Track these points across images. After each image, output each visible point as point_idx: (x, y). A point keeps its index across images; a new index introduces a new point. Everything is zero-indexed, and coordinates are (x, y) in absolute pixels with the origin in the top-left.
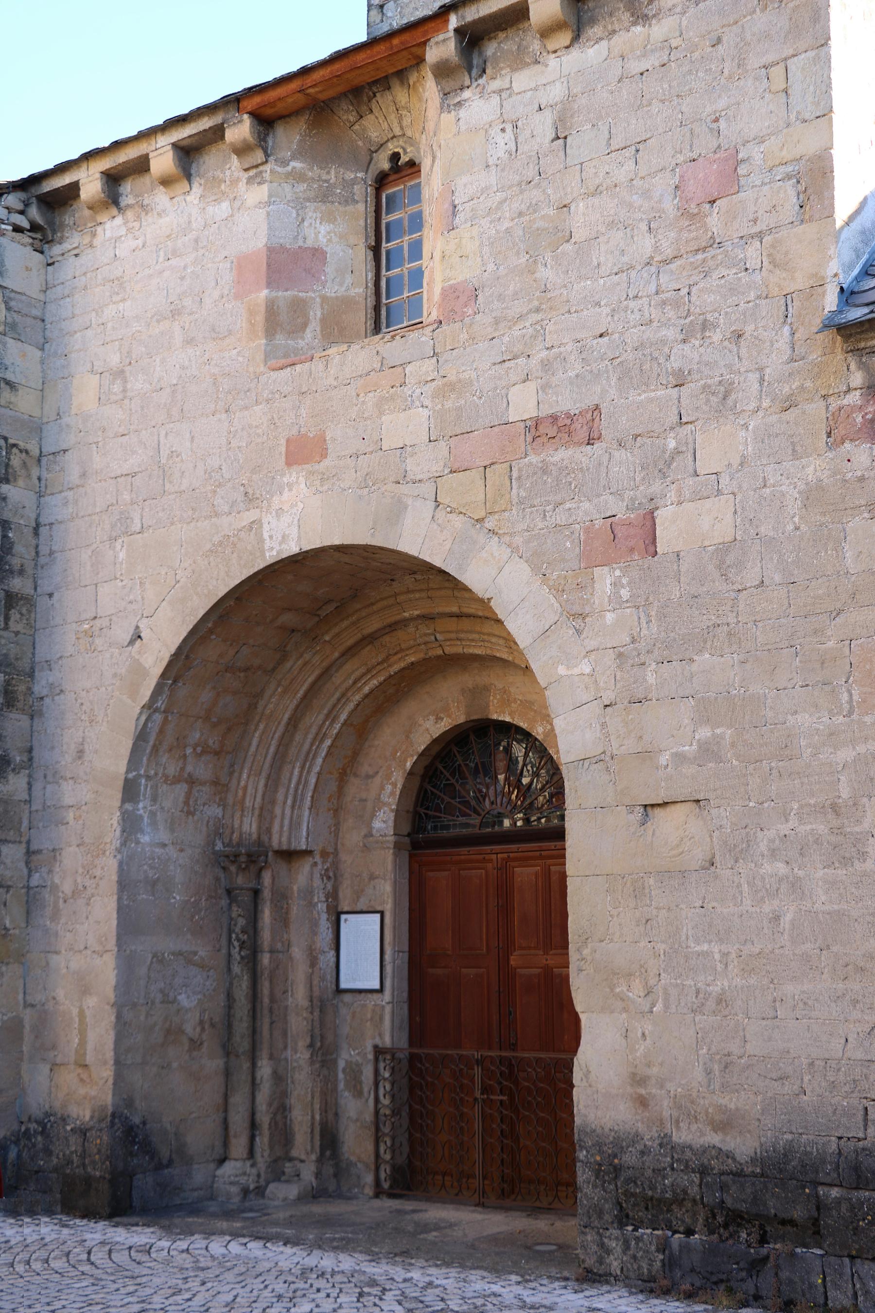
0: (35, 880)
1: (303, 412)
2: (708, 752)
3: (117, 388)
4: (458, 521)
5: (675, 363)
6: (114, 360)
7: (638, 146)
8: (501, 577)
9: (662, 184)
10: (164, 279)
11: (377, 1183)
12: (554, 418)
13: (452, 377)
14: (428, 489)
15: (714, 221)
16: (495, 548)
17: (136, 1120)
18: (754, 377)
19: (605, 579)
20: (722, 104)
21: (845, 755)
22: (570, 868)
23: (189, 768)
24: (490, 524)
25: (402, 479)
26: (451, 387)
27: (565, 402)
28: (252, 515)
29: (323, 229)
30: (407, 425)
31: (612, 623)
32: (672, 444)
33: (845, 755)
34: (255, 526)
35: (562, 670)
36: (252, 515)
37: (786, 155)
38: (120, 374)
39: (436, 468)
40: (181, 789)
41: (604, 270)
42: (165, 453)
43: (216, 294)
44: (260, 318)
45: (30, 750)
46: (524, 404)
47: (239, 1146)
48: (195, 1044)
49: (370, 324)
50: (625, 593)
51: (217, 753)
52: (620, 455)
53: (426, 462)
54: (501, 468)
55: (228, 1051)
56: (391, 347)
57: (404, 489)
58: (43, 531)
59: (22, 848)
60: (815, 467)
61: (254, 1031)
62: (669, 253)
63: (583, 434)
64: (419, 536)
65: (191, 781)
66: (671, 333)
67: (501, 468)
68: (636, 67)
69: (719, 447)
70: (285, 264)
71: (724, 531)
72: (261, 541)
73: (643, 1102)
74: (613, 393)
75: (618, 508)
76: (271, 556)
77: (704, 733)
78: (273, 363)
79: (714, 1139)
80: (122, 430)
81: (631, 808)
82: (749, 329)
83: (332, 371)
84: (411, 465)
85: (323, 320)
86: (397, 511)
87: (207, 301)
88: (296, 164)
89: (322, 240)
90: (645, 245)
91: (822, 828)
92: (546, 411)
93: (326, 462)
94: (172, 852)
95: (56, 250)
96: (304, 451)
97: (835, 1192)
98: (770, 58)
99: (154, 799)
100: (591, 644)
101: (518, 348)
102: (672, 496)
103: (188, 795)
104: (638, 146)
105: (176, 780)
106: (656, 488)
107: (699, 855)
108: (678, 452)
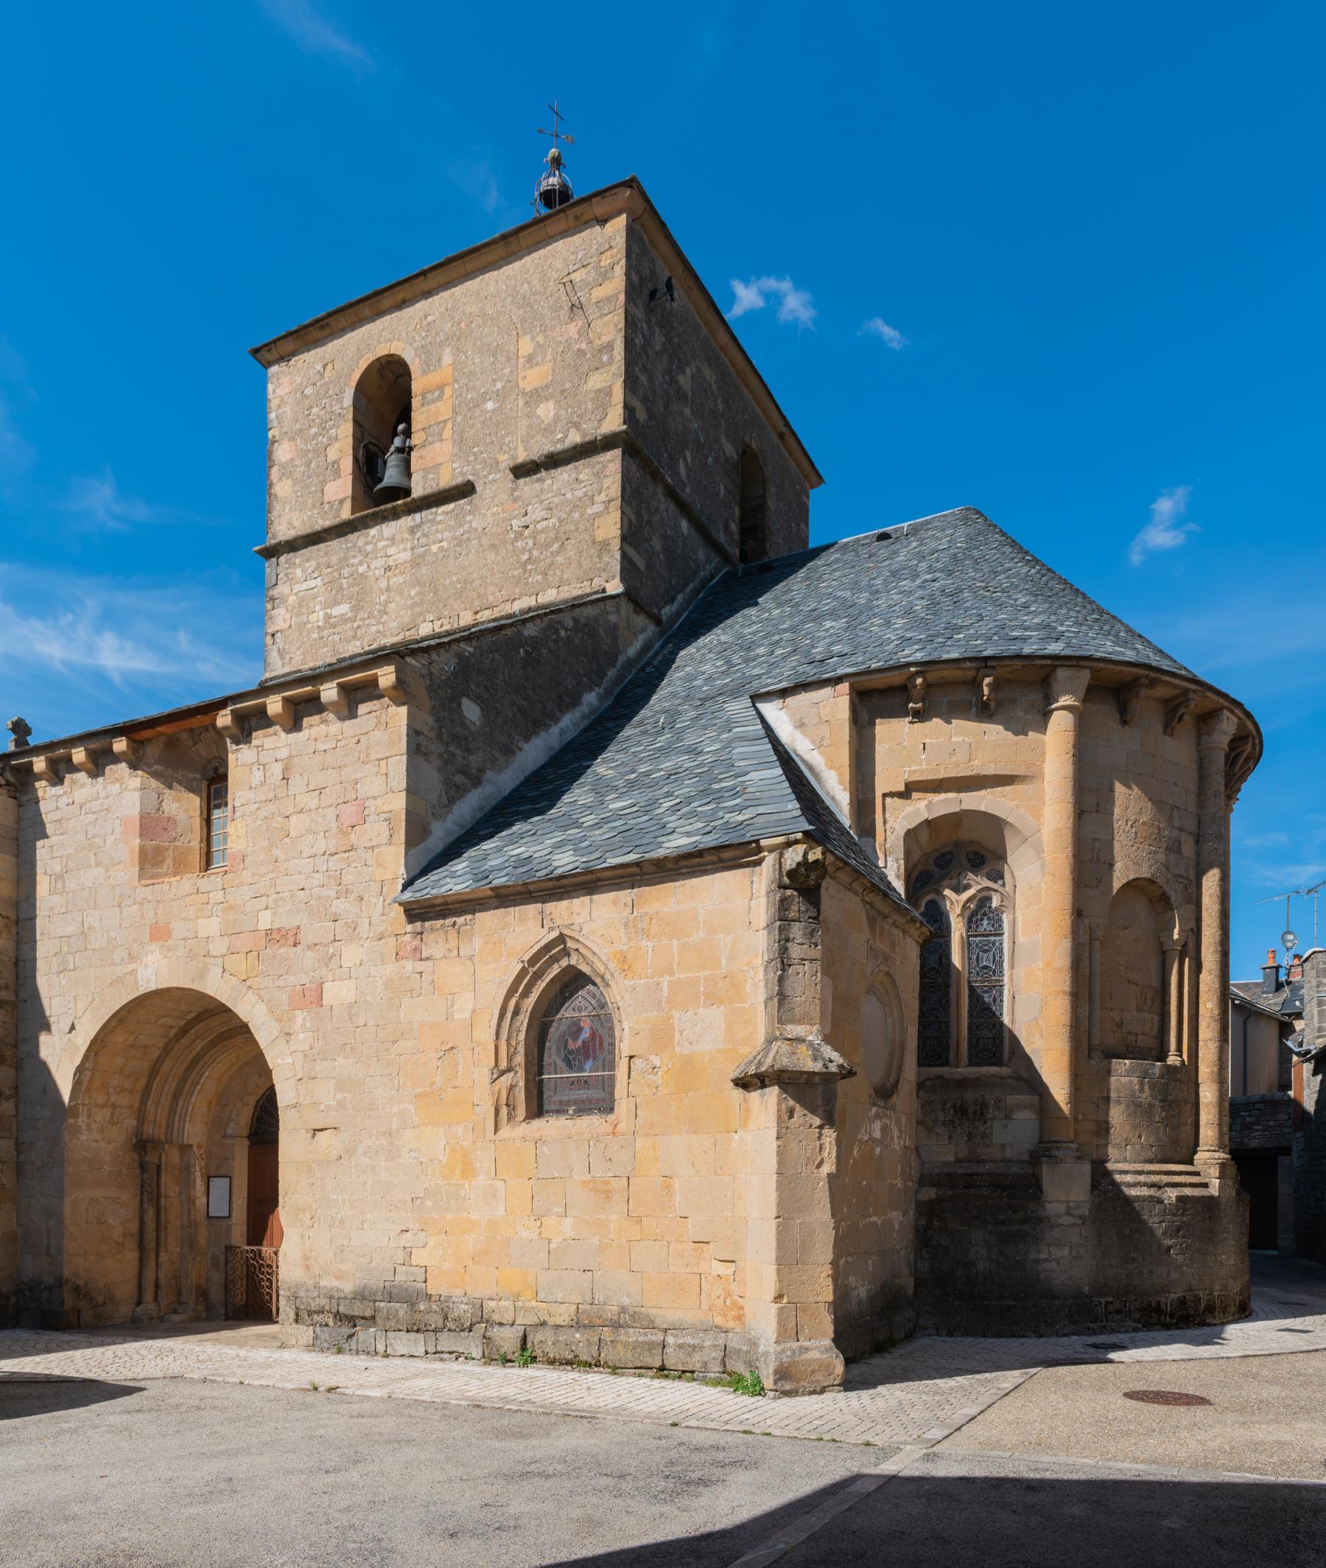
0: (22, 1158)
1: (159, 912)
2: (341, 1105)
3: (59, 885)
4: (234, 980)
5: (334, 909)
6: (58, 869)
7: (321, 791)
8: (249, 1009)
9: (331, 813)
10: (91, 819)
11: (226, 1313)
12: (279, 930)
13: (231, 903)
14: (219, 961)
15: (354, 838)
16: (251, 997)
17: (81, 1283)
18: (367, 921)
19: (300, 1015)
20: (359, 775)
21: (396, 1109)
22: (280, 1159)
23: (113, 1100)
24: (248, 983)
25: (207, 955)
26: (231, 908)
27: (284, 922)
28: (132, 966)
29: (174, 806)
30: (210, 926)
31: (302, 1039)
32: (331, 951)
33: (396, 1109)
34: (134, 972)
35: (280, 1061)
36: (132, 966)
37: (385, 808)
38: (60, 877)
39: (224, 951)
40: (108, 1111)
41: (305, 854)
42: (86, 926)
43: (113, 837)
44: (136, 855)
45: (16, 1088)
46: (265, 921)
47: (149, 1295)
48: (121, 1245)
49: (203, 863)
50: (308, 1025)
51: (131, 1092)
52: (309, 953)
53: (219, 947)
54: (254, 954)
55: (141, 1247)
56: (212, 882)
57: (209, 960)
58: (21, 964)
59: (13, 1141)
60: (390, 969)
61: (158, 1239)
62: (333, 851)
63: (291, 941)
64: (217, 987)
65: (114, 1106)
66: (333, 893)
67: (254, 954)
68: (322, 747)
69: (351, 954)
70: (150, 824)
71: (351, 997)
72: (137, 981)
73: (308, 1268)
74: (306, 921)
75: (305, 979)
76: (142, 991)
77: (339, 1096)
78: (144, 882)
79: (336, 1283)
80: (63, 910)
81: (307, 1131)
82: (366, 896)
83: (174, 891)
84: (211, 946)
85: (174, 858)
86: (203, 973)
87: (108, 842)
88: (158, 767)
89: (174, 812)
90: (321, 845)
91: (384, 1143)
92: (276, 926)
93: (170, 941)
94: (102, 1144)
95: (24, 798)
96: (159, 933)
97: (382, 1304)
98: (380, 756)
99: (89, 1116)
100: (293, 1049)
101: (262, 892)
102: (330, 977)
103: (112, 1115)
104: (321, 791)
105: (104, 1106)
106: (324, 972)
107: (335, 1154)
108: (333, 955)
